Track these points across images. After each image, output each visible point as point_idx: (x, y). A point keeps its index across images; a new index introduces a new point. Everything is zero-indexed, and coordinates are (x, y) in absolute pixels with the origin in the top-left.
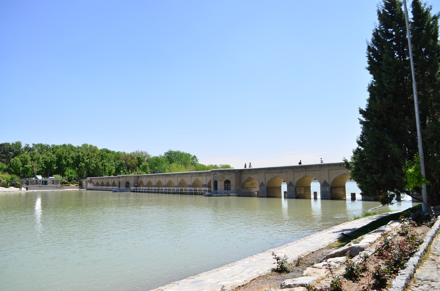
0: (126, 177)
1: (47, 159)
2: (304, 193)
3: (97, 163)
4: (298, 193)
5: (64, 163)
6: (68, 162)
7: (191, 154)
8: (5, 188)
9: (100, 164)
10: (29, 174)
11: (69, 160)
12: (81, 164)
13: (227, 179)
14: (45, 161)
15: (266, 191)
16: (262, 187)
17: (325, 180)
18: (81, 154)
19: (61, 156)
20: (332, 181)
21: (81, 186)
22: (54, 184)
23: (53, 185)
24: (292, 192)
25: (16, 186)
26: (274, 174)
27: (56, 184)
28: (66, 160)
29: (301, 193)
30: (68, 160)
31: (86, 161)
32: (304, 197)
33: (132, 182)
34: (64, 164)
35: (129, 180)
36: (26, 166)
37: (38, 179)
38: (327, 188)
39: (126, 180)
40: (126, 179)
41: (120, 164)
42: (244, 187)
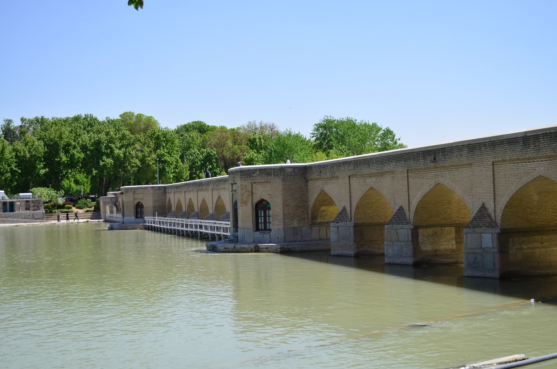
1: (22, 153)
2: (454, 247)
3: (144, 156)
4: (427, 247)
5: (64, 159)
6: (73, 156)
7: (379, 125)
9: (151, 159)
11: (75, 151)
12: (103, 161)
13: (262, 198)
14: (16, 156)
16: (340, 224)
17: (483, 204)
18: (103, 136)
19: (56, 143)
20: (503, 207)
21: (97, 213)
23: (28, 211)
24: (403, 244)
26: (369, 180)
27: (34, 210)
28: (67, 152)
29: (442, 247)
31: (117, 151)
32: (454, 260)
33: (148, 203)
34: (64, 162)
35: (142, 199)
38: (483, 235)
39: (135, 199)
40: (136, 196)
41: (206, 157)
42: (319, 220)
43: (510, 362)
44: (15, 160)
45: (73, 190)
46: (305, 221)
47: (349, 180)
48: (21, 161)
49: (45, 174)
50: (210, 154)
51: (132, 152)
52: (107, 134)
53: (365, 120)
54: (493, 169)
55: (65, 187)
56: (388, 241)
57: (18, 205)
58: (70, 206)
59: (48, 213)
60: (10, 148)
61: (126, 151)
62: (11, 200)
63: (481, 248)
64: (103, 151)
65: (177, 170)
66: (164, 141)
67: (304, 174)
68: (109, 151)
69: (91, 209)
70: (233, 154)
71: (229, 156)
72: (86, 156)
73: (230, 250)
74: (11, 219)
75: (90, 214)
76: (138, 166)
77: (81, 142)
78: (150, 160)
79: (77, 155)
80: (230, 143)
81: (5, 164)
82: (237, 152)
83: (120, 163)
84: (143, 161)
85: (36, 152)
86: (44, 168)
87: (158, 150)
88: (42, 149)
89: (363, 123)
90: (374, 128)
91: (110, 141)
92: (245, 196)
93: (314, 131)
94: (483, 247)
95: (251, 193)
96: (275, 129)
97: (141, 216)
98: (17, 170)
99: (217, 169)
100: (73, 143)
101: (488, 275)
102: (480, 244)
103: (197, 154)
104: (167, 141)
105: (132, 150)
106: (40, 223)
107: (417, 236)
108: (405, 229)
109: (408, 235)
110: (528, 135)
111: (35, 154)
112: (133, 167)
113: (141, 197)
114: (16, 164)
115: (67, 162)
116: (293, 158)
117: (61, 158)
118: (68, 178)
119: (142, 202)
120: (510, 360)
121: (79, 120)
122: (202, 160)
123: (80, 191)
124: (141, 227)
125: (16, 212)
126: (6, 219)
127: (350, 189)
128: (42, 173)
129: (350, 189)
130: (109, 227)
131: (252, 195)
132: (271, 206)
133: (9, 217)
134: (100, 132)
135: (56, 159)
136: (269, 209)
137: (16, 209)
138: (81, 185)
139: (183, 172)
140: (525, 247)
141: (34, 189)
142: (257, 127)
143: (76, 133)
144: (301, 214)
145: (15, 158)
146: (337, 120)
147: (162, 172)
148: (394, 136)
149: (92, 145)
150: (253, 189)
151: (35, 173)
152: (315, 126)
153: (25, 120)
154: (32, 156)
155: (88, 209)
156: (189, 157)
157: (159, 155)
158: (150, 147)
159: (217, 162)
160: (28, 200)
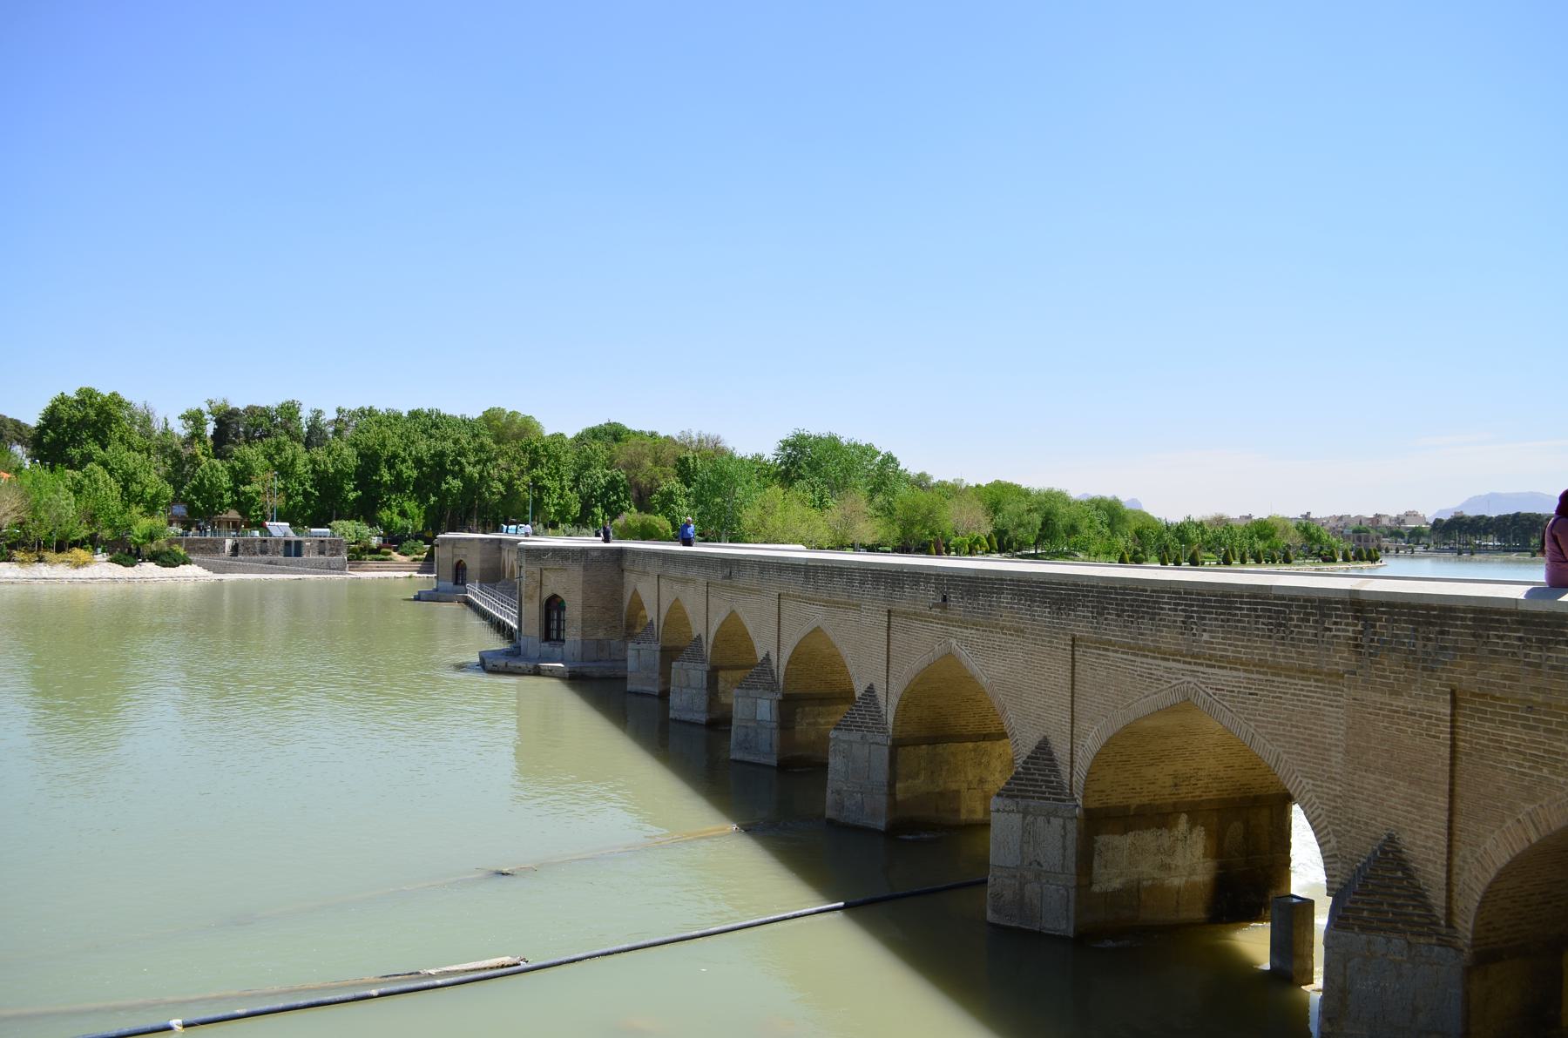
0: (454, 544)
1: (323, 466)
5: (387, 477)
6: (400, 474)
7: (877, 447)
8: (124, 566)
12: (447, 483)
13: (555, 592)
14: (314, 471)
18: (449, 445)
23: (322, 557)
25: (163, 561)
27: (332, 555)
28: (391, 467)
30: (400, 466)
31: (468, 469)
33: (474, 563)
34: (386, 482)
35: (465, 556)
36: (242, 488)
37: (271, 536)
38: (759, 701)
39: (454, 556)
40: (457, 551)
41: (609, 483)
45: (396, 526)
51: (492, 472)
52: (456, 442)
53: (855, 438)
60: (306, 456)
62: (297, 538)
64: (448, 467)
65: (561, 501)
67: (618, 559)
68: (457, 468)
69: (421, 557)
70: (652, 480)
71: (644, 483)
73: (500, 669)
75: (418, 565)
76: (500, 493)
77: (414, 453)
80: (648, 463)
83: (472, 488)
84: (509, 485)
85: (345, 465)
86: (355, 490)
88: (351, 458)
91: (460, 453)
93: (778, 450)
94: (758, 718)
100: (403, 454)
101: (763, 761)
104: (549, 457)
107: (716, 682)
110: (809, 564)
112: (493, 493)
114: (312, 483)
115: (391, 483)
117: (381, 476)
118: (389, 508)
119: (464, 560)
120: (491, 966)
122: (603, 487)
123: (407, 529)
124: (461, 600)
125: (305, 557)
126: (287, 567)
131: (541, 587)
132: (567, 606)
136: (564, 609)
137: (303, 552)
138: (408, 519)
140: (822, 721)
141: (334, 523)
142: (694, 439)
144: (610, 620)
145: (312, 473)
147: (538, 503)
149: (432, 457)
153: (344, 411)
155: (416, 556)
158: (522, 465)
159: (625, 491)
160: (322, 539)
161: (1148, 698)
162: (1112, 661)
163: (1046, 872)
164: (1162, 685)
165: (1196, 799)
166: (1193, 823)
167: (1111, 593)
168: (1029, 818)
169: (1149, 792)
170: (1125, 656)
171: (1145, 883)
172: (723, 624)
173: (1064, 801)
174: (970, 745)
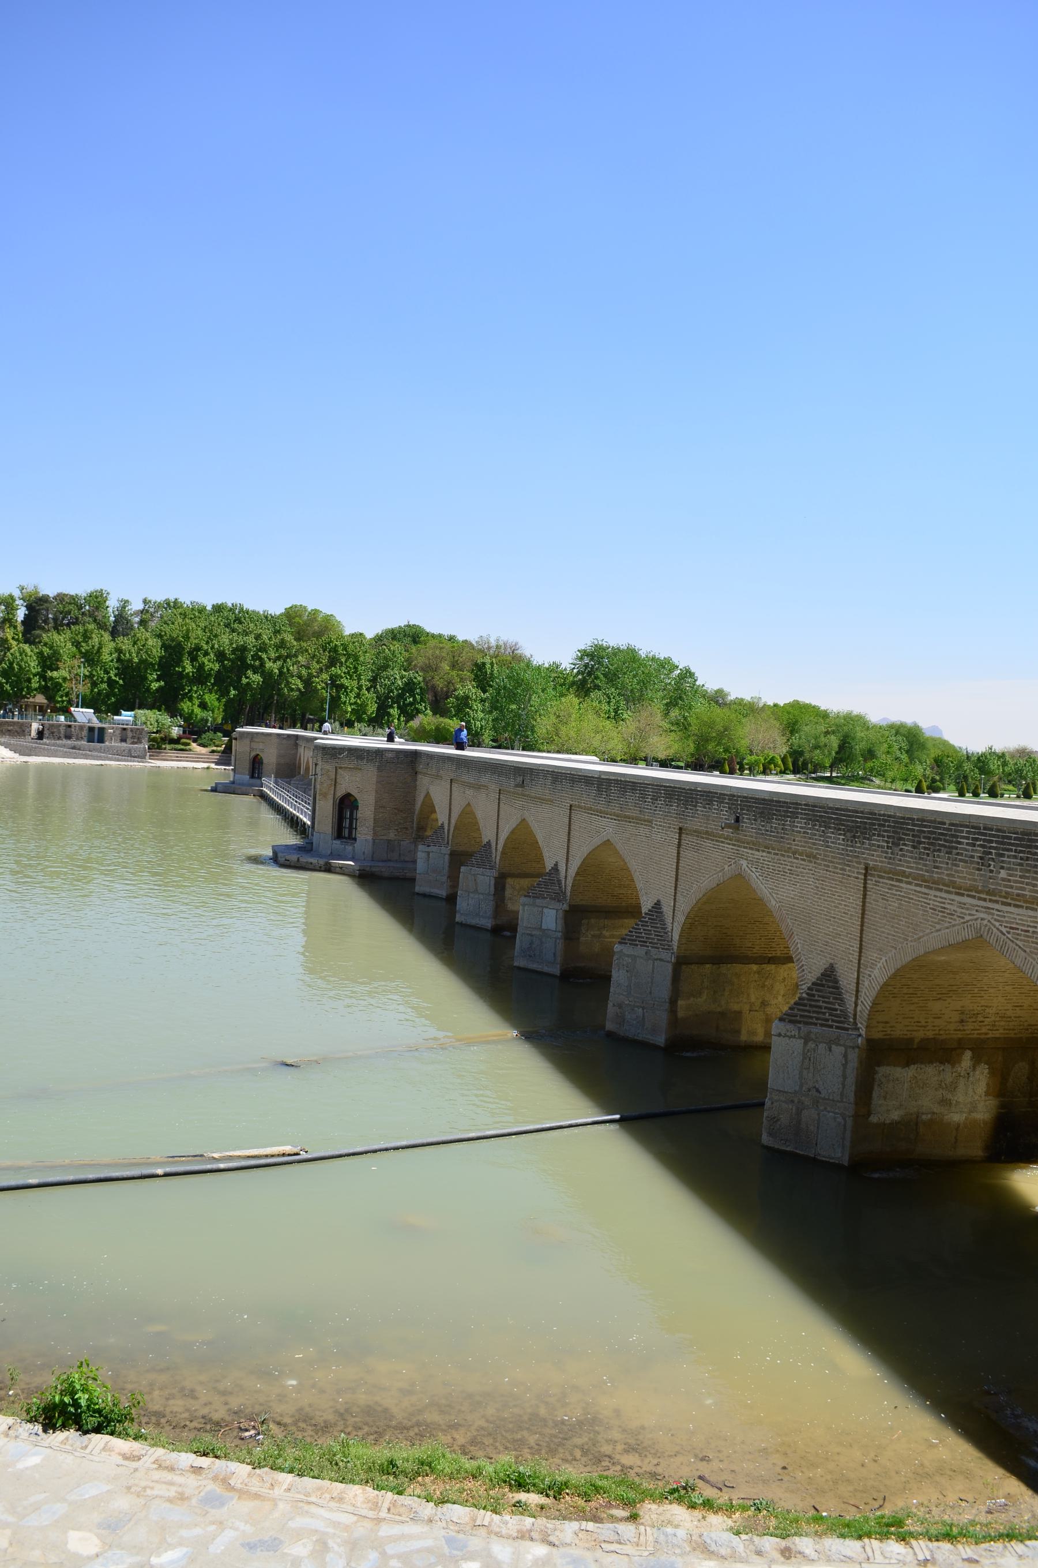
1: (127, 655)
3: (310, 676)
6: (202, 666)
7: (675, 661)
9: (320, 682)
10: (59, 702)
12: (247, 678)
14: (119, 660)
15: (447, 868)
18: (250, 640)
19: (179, 644)
22: (128, 740)
23: (124, 744)
24: (481, 897)
27: (133, 743)
28: (193, 659)
31: (269, 665)
33: (270, 757)
34: (188, 673)
35: (262, 750)
36: (49, 674)
37: (75, 721)
39: (252, 749)
40: (254, 745)
41: (406, 684)
43: (289, 1155)
44: (116, 665)
45: (196, 718)
46: (408, 832)
47: (451, 786)
48: (126, 668)
49: (158, 690)
50: (412, 680)
51: (291, 668)
52: (258, 637)
54: (570, 815)
55: (184, 711)
56: (462, 890)
57: (110, 733)
58: (188, 741)
59: (155, 749)
60: (112, 645)
61: (283, 666)
62: (100, 725)
63: (540, 928)
64: (249, 662)
65: (358, 701)
66: (345, 655)
67: (412, 762)
68: (257, 663)
70: (449, 683)
72: (223, 668)
73: (292, 864)
74: (96, 753)
75: (216, 756)
76: (299, 690)
77: (216, 646)
78: (319, 683)
79: (208, 665)
80: (446, 667)
81: (101, 670)
82: (453, 681)
84: (308, 682)
85: (149, 656)
86: (158, 680)
87: (333, 669)
89: (651, 655)
90: (666, 665)
92: (325, 785)
94: (543, 928)
95: (333, 783)
96: (519, 652)
97: (258, 775)
98: (118, 679)
99: (421, 705)
100: (205, 647)
102: (539, 923)
103: (397, 677)
104: (348, 656)
105: (293, 665)
106: (138, 764)
107: (503, 889)
108: (487, 876)
109: (490, 885)
110: (603, 777)
111: (146, 659)
113: (261, 747)
114: (117, 671)
115: (193, 675)
116: (529, 700)
117: (184, 668)
121: (222, 612)
123: (207, 721)
126: (90, 753)
127: (450, 799)
128: (154, 688)
129: (450, 799)
130: (212, 787)
131: (335, 785)
133: (94, 750)
134: (247, 633)
135: (177, 669)
136: (357, 808)
137: (106, 738)
138: (208, 712)
139: (367, 704)
140: (606, 933)
143: (211, 631)
145: (117, 662)
146: (613, 647)
147: (335, 702)
148: (696, 680)
149: (234, 651)
150: (338, 777)
151: (144, 686)
152: (578, 653)
153: (150, 601)
154: (141, 661)
155: (215, 748)
156: (385, 680)
157: (333, 675)
158: (321, 663)
159: (421, 694)
160: (125, 726)
161: (940, 933)
162: (905, 893)
163: (824, 1099)
164: (955, 920)
165: (983, 1036)
166: (977, 1060)
167: (908, 824)
168: (811, 1045)
169: (934, 1026)
170: (918, 889)
171: (924, 1117)
172: (513, 832)
173: (847, 1029)
174: (755, 967)
